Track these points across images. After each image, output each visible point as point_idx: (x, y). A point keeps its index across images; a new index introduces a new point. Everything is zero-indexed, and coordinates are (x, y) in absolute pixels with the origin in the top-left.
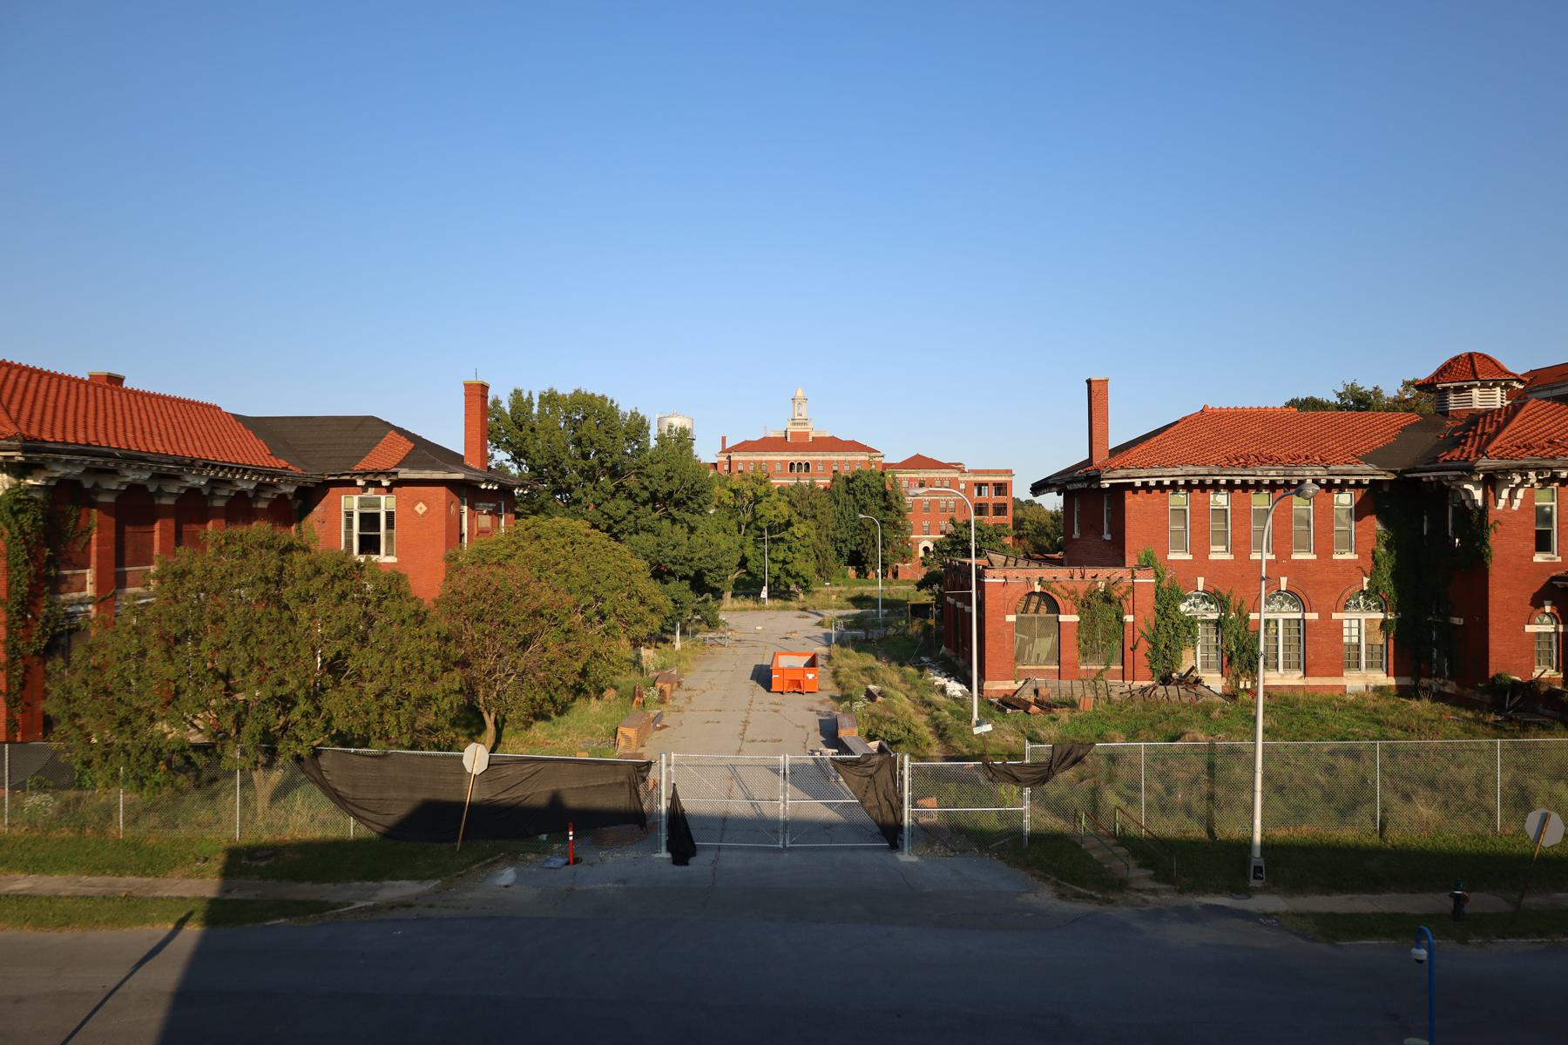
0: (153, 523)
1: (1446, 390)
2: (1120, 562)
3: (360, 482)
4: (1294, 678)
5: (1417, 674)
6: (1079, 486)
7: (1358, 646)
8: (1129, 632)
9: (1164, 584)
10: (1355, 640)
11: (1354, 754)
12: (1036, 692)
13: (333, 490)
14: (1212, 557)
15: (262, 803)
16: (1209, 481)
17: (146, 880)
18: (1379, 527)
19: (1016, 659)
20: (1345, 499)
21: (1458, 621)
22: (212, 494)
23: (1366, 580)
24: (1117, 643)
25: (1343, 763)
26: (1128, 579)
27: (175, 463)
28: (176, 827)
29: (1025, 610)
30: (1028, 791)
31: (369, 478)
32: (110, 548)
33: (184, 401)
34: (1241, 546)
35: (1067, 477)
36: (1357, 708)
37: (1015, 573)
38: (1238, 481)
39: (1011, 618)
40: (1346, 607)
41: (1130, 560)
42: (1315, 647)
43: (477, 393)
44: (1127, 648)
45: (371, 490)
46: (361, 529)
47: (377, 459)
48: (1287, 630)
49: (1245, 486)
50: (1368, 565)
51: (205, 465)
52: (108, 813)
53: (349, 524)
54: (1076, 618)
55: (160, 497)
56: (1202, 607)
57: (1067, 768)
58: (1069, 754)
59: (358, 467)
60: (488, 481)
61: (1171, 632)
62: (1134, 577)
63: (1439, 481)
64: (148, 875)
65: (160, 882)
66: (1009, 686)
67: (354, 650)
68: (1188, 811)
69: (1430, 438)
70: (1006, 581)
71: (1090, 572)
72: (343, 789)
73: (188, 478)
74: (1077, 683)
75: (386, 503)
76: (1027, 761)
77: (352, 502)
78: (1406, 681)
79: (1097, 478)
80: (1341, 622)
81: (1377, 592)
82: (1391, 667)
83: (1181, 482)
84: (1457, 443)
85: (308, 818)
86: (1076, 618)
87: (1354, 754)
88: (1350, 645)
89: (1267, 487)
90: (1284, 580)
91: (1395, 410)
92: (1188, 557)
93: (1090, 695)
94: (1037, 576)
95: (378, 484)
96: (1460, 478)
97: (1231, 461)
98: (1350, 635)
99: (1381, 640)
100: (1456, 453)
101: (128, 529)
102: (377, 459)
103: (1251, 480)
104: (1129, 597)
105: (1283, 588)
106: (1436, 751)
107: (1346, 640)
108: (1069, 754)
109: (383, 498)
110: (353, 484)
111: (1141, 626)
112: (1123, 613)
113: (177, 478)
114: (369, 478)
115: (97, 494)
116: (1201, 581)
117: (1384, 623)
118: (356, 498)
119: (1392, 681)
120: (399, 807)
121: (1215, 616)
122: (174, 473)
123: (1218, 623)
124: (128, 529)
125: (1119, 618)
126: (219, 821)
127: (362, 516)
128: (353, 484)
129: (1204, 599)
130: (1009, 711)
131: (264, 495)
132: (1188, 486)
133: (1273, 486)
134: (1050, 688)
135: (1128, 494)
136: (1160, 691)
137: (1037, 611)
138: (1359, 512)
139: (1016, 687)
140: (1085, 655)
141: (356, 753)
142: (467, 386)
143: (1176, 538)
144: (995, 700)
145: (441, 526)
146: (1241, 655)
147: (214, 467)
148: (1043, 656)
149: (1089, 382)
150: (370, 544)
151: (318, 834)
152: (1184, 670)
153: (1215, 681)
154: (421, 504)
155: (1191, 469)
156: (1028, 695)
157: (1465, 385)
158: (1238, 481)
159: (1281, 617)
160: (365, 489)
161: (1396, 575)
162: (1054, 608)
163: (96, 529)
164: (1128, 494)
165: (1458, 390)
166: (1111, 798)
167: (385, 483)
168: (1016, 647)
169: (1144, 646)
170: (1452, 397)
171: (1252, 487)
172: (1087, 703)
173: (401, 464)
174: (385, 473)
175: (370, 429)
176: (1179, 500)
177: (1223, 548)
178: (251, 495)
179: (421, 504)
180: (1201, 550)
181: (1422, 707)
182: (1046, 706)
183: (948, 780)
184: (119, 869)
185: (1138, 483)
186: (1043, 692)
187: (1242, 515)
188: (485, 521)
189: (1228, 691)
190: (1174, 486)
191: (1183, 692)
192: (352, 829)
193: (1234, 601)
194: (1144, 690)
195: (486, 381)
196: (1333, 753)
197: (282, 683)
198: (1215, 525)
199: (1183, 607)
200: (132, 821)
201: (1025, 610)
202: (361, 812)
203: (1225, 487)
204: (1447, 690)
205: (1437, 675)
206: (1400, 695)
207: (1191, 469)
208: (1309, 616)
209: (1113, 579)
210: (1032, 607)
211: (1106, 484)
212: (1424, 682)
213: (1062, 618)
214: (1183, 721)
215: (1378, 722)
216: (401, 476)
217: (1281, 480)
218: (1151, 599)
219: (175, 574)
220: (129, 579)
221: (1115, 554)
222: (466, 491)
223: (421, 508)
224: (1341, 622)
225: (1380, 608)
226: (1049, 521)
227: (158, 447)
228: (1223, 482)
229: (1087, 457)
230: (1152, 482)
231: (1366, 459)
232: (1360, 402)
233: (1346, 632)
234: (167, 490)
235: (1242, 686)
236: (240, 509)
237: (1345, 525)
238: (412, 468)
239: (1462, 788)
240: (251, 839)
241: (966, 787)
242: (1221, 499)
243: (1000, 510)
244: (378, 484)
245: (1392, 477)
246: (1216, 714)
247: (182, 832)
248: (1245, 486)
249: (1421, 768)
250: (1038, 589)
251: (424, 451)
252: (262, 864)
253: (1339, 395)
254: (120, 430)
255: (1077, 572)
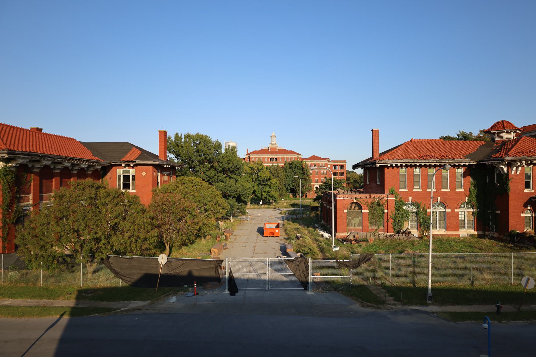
0: (52, 179)
1: (494, 133)
2: (383, 192)
3: (123, 165)
4: (442, 232)
5: (484, 230)
6: (369, 166)
7: (464, 221)
8: (386, 216)
9: (398, 200)
10: (463, 219)
11: (463, 258)
12: (354, 236)
13: (114, 167)
14: (414, 190)
15: (90, 274)
16: (413, 164)
17: (50, 300)
18: (472, 180)
19: (347, 225)
20: (460, 171)
21: (498, 212)
22: (72, 169)
23: (467, 198)
24: (382, 220)
25: (459, 261)
26: (385, 198)
27: (60, 158)
28: (60, 282)
29: (351, 208)
30: (351, 270)
31: (126, 163)
32: (38, 187)
33: (63, 137)
34: (424, 187)
35: (365, 163)
36: (464, 242)
37: (347, 196)
38: (423, 164)
39: (346, 211)
40: (460, 207)
41: (386, 191)
42: (450, 221)
43: (163, 134)
44: (385, 221)
45: (127, 167)
46: (124, 181)
47: (129, 157)
48: (440, 215)
49: (426, 166)
50: (468, 193)
51: (70, 159)
52: (37, 278)
53: (119, 179)
54: (368, 211)
55: (55, 170)
56: (411, 207)
57: (365, 262)
58: (365, 257)
59: (123, 160)
60: (167, 164)
61: (400, 216)
62: (388, 197)
63: (492, 164)
64: (51, 299)
65: (55, 301)
66: (345, 234)
67: (121, 222)
68: (406, 277)
69: (489, 150)
70: (344, 198)
71: (373, 195)
72: (117, 270)
73: (64, 163)
74: (368, 233)
75: (132, 172)
76: (351, 260)
77: (120, 172)
78: (481, 233)
79: (375, 163)
80: (458, 212)
81: (471, 202)
82: (476, 228)
83: (404, 165)
84: (498, 151)
85: (105, 280)
86: (368, 211)
87: (463, 258)
88: (461, 220)
89: (433, 166)
90: (439, 198)
91: (477, 140)
92: (406, 190)
93: (373, 237)
94: (354, 197)
95: (129, 166)
96: (499, 163)
97: (421, 157)
98: (461, 217)
99: (472, 219)
100: (498, 155)
101: (44, 181)
102: (129, 157)
103: (428, 164)
104: (386, 204)
105: (439, 201)
106: (491, 257)
107: (460, 219)
108: (365, 257)
109: (131, 170)
110: (121, 165)
111: (390, 214)
112: (384, 210)
113: (61, 163)
114: (126, 163)
115: (33, 169)
116: (410, 199)
117: (473, 213)
118: (122, 170)
119: (476, 233)
120: (136, 276)
121: (415, 211)
122: (59, 161)
123: (416, 213)
124: (44, 181)
125: (383, 211)
126: (75, 280)
127: (124, 176)
128: (121, 165)
129: (412, 205)
130: (345, 243)
131: (90, 169)
132: (406, 166)
133: (435, 166)
134: (359, 235)
135: (386, 169)
136: (397, 236)
137: (354, 209)
138: (465, 175)
139: (347, 235)
140: (371, 224)
141: (122, 257)
142: (160, 132)
143: (402, 184)
144: (340, 239)
145: (151, 180)
146: (424, 224)
147: (73, 159)
148: (357, 224)
149: (372, 130)
150: (126, 186)
151: (109, 285)
152: (405, 229)
153: (415, 233)
154: (144, 172)
155: (407, 160)
156: (351, 238)
157: (501, 132)
158: (423, 164)
159: (438, 211)
160: (125, 167)
161: (477, 197)
162: (360, 208)
163: (33, 181)
164: (386, 169)
165: (498, 133)
166: (380, 273)
167: (132, 165)
168: (347, 221)
169: (391, 221)
170: (496, 136)
171: (428, 166)
172: (372, 240)
173: (137, 159)
174: (132, 162)
175: (127, 147)
176: (403, 171)
177: (418, 187)
178: (86, 169)
179: (144, 172)
180: (410, 188)
181: (486, 241)
182: (358, 241)
183: (324, 267)
184: (41, 297)
185: (389, 165)
186: (356, 237)
187: (425, 176)
188: (166, 178)
189: (420, 236)
190: (401, 166)
191: (404, 236)
192: (120, 283)
193: (422, 205)
194: (391, 236)
195: (166, 130)
196: (456, 257)
197: (96, 233)
198: (415, 179)
199: (404, 208)
200: (45, 281)
201: (351, 208)
202: (123, 278)
203: (419, 166)
204: (495, 236)
205: (491, 231)
206: (479, 238)
207: (407, 160)
208: (447, 210)
209: (381, 198)
210: (353, 207)
211: (378, 165)
212: (487, 233)
213: (363, 211)
214: (404, 246)
215: (471, 247)
216: (137, 163)
217: (438, 164)
218: (394, 205)
219: (60, 196)
220: (44, 198)
221: (381, 189)
222: (159, 168)
223: (144, 174)
224: (458, 212)
225: (472, 208)
226: (359, 178)
227: (54, 153)
228: (418, 165)
229: (371, 156)
230: (394, 165)
231: (467, 157)
232: (465, 137)
233: (460, 216)
234: (57, 167)
235: (424, 234)
236: (82, 174)
237: (460, 179)
238: (141, 160)
239: (500, 269)
240: (86, 287)
241: (330, 269)
242: (417, 171)
243: (342, 174)
244: (129, 166)
245: (476, 163)
246: (416, 244)
247: (62, 284)
248: (426, 166)
249: (486, 262)
250: (355, 201)
251: (145, 154)
252: (90, 295)
253: (458, 135)
254: (41, 147)
255: (368, 195)
